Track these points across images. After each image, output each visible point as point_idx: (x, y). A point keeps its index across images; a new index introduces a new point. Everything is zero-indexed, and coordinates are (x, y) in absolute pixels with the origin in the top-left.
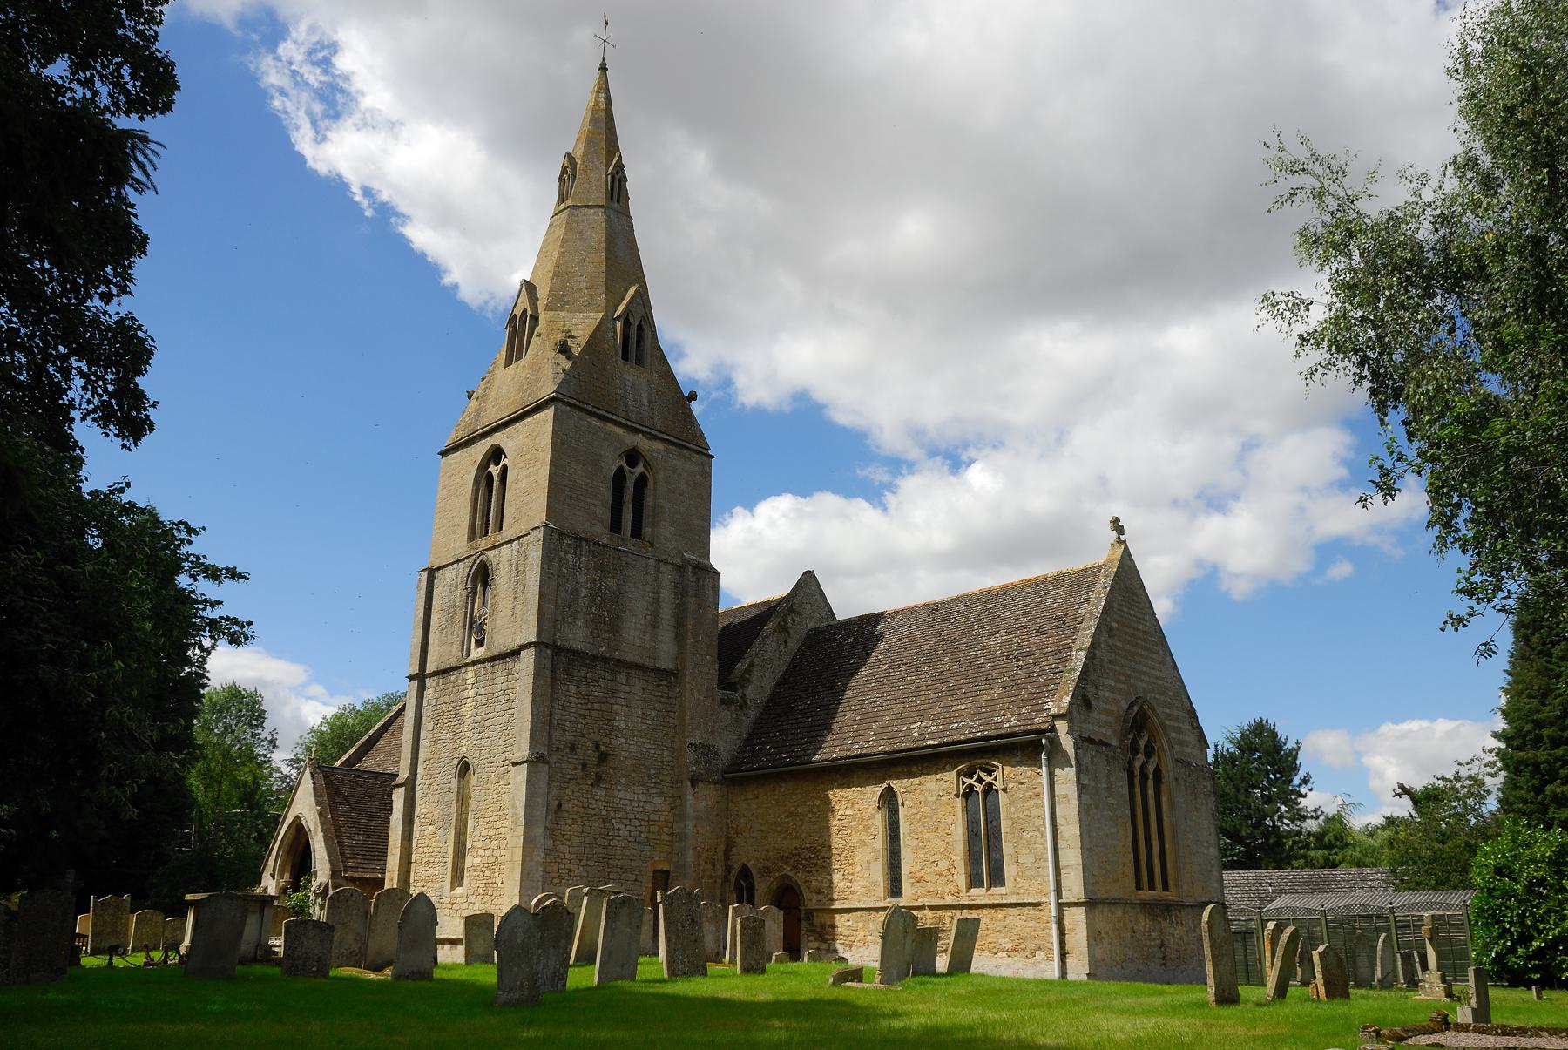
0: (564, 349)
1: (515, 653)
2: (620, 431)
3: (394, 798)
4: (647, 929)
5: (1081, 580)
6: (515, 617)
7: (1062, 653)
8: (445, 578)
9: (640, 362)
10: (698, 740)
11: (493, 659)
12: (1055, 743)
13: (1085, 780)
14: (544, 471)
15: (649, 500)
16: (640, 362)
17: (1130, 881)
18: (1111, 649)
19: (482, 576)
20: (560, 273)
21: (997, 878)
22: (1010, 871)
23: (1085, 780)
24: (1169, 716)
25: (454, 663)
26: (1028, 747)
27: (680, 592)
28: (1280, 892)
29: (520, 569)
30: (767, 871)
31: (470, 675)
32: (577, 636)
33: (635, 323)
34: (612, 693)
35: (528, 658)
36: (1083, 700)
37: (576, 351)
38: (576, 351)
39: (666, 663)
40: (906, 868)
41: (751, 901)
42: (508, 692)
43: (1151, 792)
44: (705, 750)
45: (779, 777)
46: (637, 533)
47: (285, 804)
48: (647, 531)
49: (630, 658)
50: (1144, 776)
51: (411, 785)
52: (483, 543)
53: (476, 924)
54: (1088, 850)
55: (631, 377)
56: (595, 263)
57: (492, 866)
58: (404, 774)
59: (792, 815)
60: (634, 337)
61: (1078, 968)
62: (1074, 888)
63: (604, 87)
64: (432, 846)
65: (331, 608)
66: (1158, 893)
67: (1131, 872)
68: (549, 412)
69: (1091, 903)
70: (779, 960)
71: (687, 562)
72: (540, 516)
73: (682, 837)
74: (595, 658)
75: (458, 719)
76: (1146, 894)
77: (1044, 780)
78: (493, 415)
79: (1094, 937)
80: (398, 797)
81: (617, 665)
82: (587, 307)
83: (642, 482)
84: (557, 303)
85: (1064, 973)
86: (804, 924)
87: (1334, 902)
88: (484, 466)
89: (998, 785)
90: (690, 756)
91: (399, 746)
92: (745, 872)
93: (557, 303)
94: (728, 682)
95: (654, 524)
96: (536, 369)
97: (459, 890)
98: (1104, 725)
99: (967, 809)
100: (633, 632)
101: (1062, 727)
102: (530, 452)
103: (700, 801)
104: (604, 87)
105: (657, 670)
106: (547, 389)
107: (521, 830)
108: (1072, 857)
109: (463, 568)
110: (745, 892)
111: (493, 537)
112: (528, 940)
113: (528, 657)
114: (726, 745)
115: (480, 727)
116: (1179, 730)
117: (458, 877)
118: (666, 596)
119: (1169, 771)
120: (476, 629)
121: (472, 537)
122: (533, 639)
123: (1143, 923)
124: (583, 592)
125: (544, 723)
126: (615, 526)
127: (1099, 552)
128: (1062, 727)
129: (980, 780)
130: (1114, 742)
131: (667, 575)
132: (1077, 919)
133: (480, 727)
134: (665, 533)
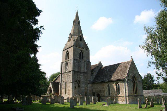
0: (74, 40)
1: (70, 71)
2: (80, 48)
3: (72, 56)
4: (84, 99)
5: (127, 63)
6: (70, 68)
7: (126, 70)
8: (63, 64)
9: (82, 41)
10: (89, 79)
11: (68, 72)
12: (125, 80)
13: (128, 84)
14: (73, 53)
15: (83, 55)
16: (82, 41)
17: (133, 93)
18: (131, 70)
19: (67, 64)
20: (73, 32)
21: (119, 94)
22: (121, 93)
23: (128, 84)
24: (137, 76)
25: (64, 72)
26: (122, 80)
27: (87, 65)
28: (151, 92)
29: (71, 63)
30: (96, 92)
31: (66, 73)
32: (76, 70)
33: (81, 37)
34: (80, 75)
35: (72, 72)
36: (128, 75)
37: (75, 40)
38: (75, 40)
39: (85, 72)
40: (110, 93)
41: (95, 96)
42: (70, 75)
43: (135, 84)
44: (90, 81)
45: (97, 83)
46: (82, 59)
47: (48, 86)
48: (83, 58)
49: (82, 71)
50: (134, 82)
51: (61, 84)
52: (67, 60)
53: (68, 99)
54: (128, 91)
55: (81, 43)
56: (77, 31)
57: (69, 92)
58: (60, 83)
59: (99, 87)
60: (81, 38)
61: (128, 103)
62: (127, 95)
63: (77, 12)
64: (63, 90)
65: (50, 58)
66: (136, 95)
67: (133, 92)
68: (73, 47)
69: (129, 96)
70: (97, 102)
71: (87, 61)
72: (72, 58)
73: (88, 89)
74: (78, 72)
75: (65, 78)
76: (135, 95)
77: (124, 84)
78: (67, 47)
79: (129, 99)
80: (60, 85)
81: (81, 72)
82: (76, 36)
83: (82, 53)
84: (74, 35)
85: (126, 103)
86: (100, 98)
87: (156, 94)
88: (67, 52)
89: (119, 84)
90: (88, 81)
91: (59, 79)
92: (94, 93)
93: (74, 35)
94: (92, 73)
95: (84, 58)
96: (72, 42)
97: (66, 95)
98: (130, 78)
99: (116, 87)
100: (82, 69)
101: (126, 78)
102: (71, 51)
103: (89, 86)
104: (77, 12)
105: (85, 73)
106: (73, 45)
107: (72, 89)
108: (127, 91)
109: (65, 63)
110: (94, 95)
111: (68, 60)
112: (73, 101)
113: (72, 72)
114: (92, 80)
115: (67, 79)
116: (138, 78)
117: (66, 94)
118: (85, 65)
119: (137, 82)
120: (66, 69)
121: (66, 60)
122: (72, 70)
123: (134, 98)
124: (77, 65)
125: (73, 79)
126: (80, 58)
127: (129, 59)
128: (126, 78)
129: (118, 84)
130: (131, 79)
131: (85, 63)
132: (127, 98)
133: (67, 79)
134: (85, 58)
